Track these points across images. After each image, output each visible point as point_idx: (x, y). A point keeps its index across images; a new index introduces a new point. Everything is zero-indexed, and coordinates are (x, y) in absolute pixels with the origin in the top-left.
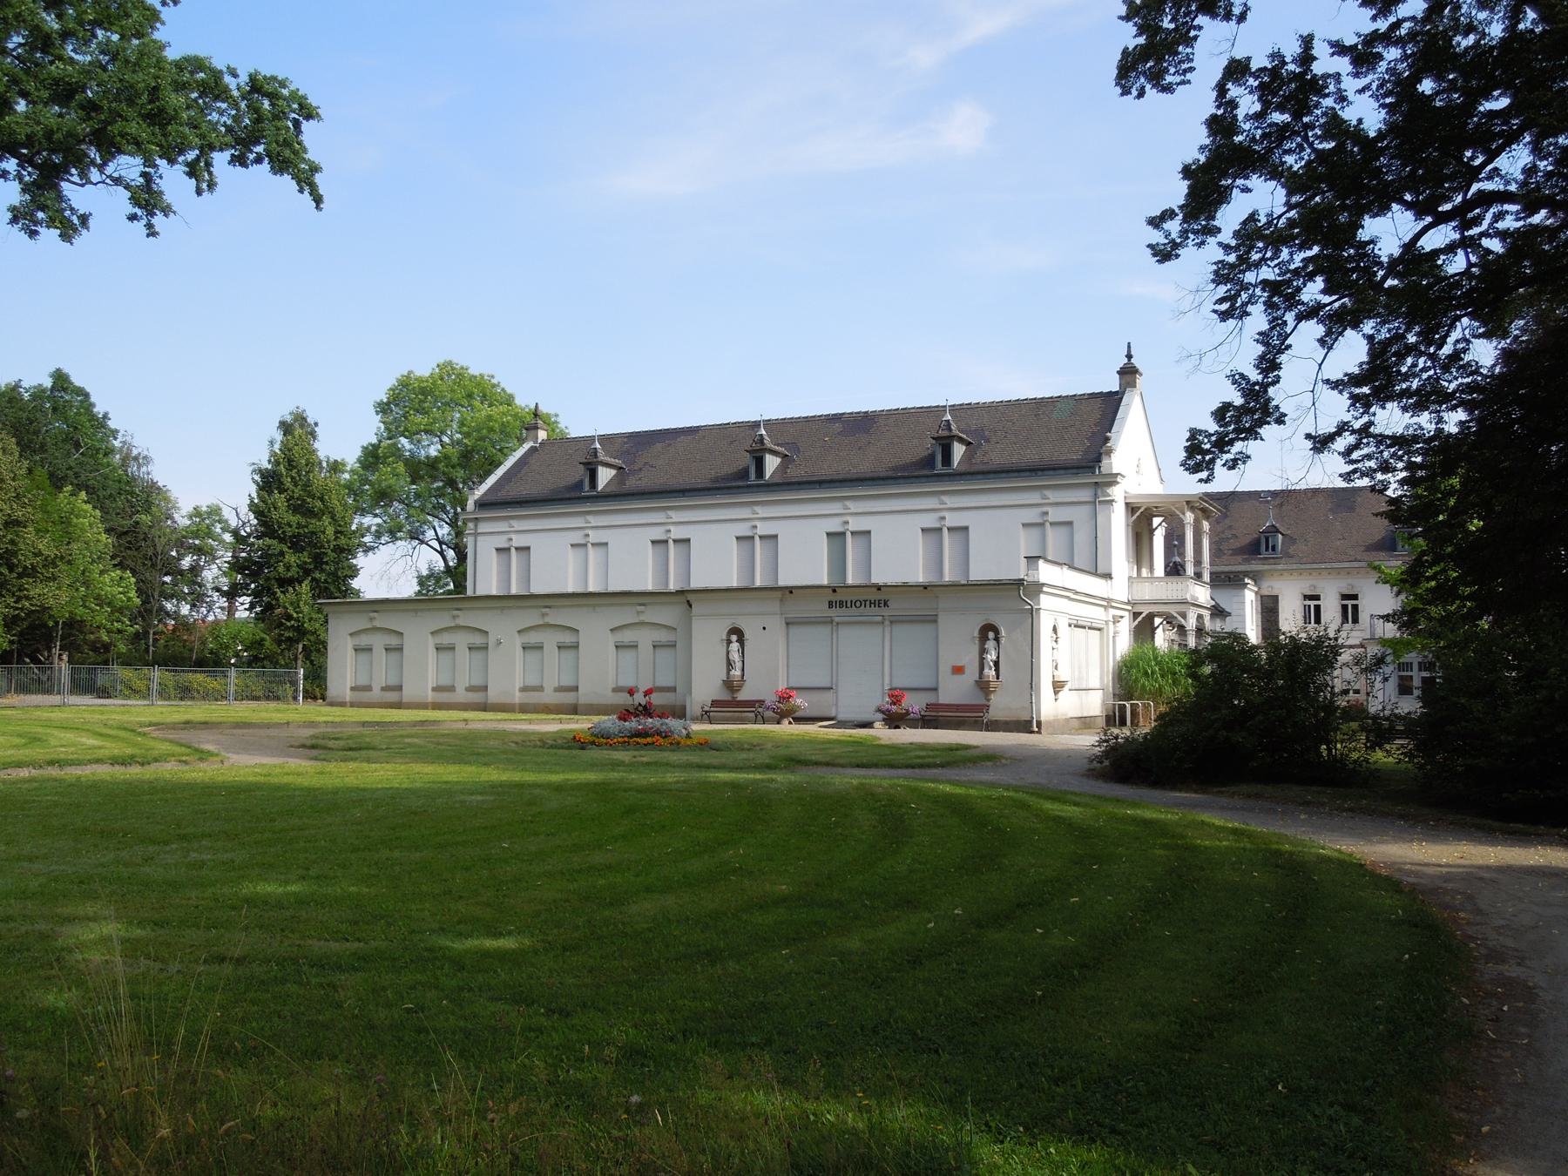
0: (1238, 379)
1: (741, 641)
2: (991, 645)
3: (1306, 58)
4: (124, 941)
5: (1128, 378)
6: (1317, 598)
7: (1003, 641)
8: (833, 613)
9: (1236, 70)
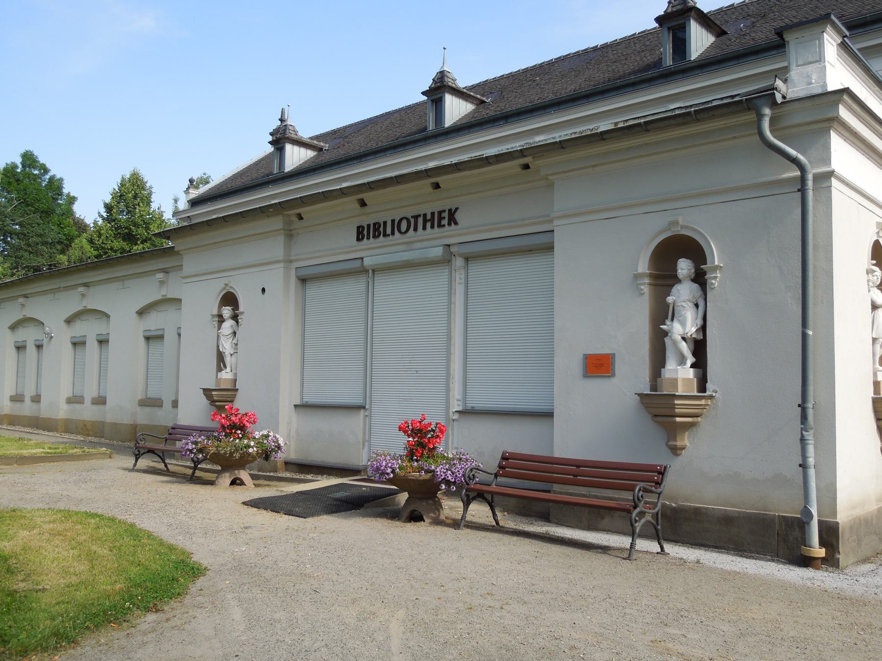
2: (683, 294)
4: (676, 380)
7: (715, 281)
8: (374, 253)
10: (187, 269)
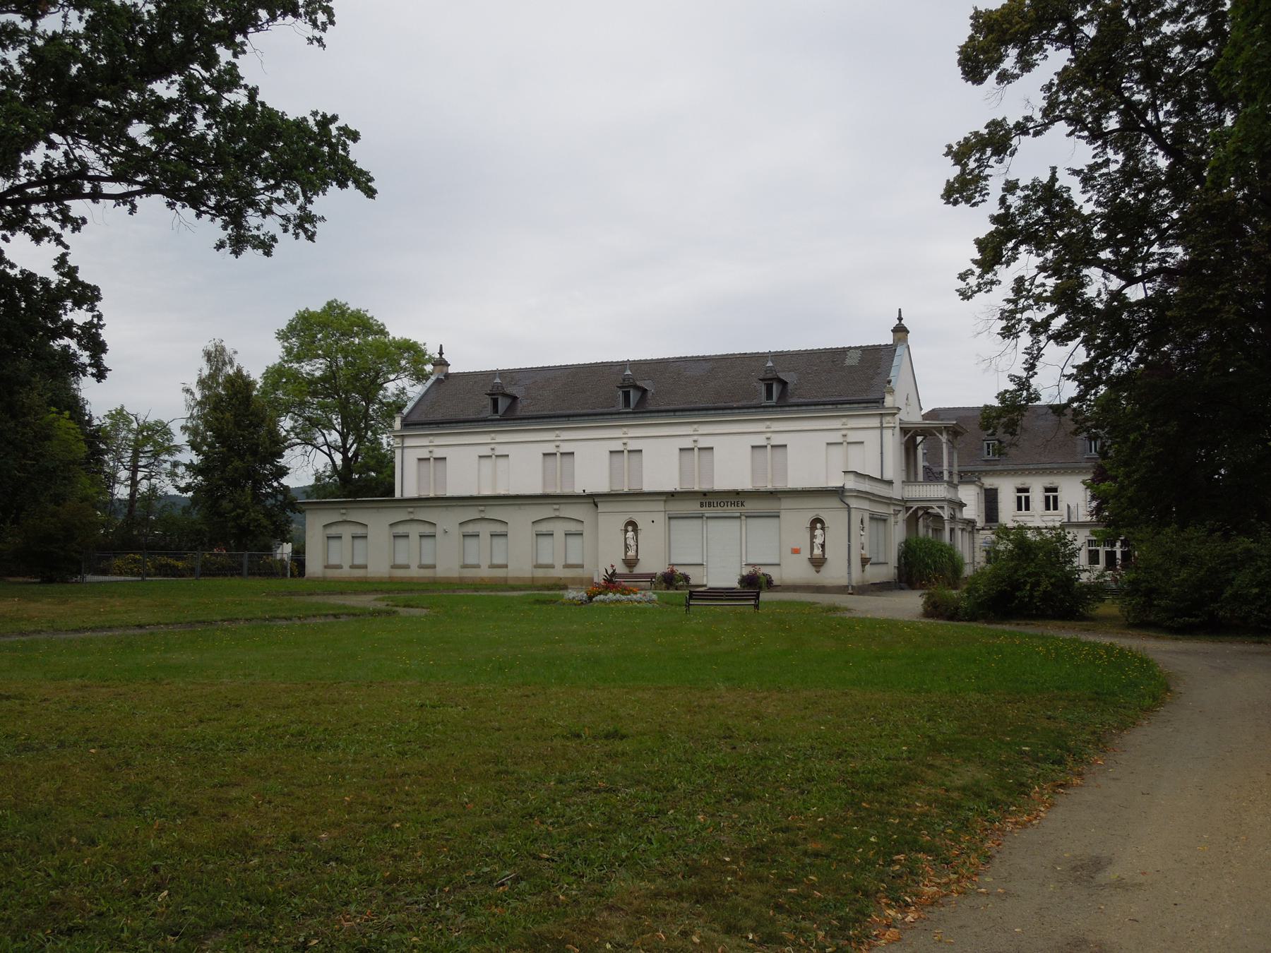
0: (1012, 378)
1: (635, 530)
2: (818, 532)
3: (1053, 179)
5: (900, 335)
6: (1027, 490)
9: (1011, 187)
10: (978, 413)
